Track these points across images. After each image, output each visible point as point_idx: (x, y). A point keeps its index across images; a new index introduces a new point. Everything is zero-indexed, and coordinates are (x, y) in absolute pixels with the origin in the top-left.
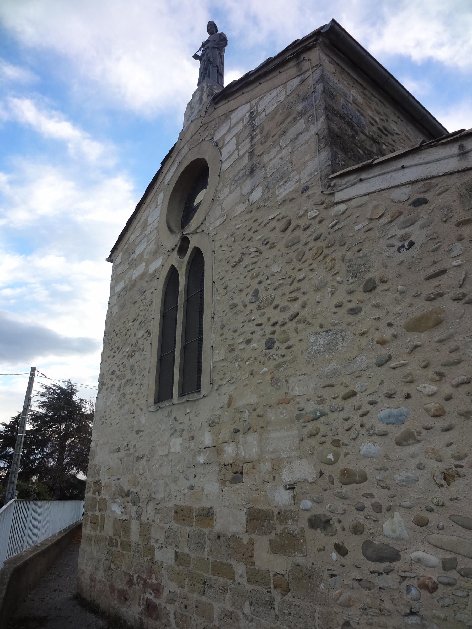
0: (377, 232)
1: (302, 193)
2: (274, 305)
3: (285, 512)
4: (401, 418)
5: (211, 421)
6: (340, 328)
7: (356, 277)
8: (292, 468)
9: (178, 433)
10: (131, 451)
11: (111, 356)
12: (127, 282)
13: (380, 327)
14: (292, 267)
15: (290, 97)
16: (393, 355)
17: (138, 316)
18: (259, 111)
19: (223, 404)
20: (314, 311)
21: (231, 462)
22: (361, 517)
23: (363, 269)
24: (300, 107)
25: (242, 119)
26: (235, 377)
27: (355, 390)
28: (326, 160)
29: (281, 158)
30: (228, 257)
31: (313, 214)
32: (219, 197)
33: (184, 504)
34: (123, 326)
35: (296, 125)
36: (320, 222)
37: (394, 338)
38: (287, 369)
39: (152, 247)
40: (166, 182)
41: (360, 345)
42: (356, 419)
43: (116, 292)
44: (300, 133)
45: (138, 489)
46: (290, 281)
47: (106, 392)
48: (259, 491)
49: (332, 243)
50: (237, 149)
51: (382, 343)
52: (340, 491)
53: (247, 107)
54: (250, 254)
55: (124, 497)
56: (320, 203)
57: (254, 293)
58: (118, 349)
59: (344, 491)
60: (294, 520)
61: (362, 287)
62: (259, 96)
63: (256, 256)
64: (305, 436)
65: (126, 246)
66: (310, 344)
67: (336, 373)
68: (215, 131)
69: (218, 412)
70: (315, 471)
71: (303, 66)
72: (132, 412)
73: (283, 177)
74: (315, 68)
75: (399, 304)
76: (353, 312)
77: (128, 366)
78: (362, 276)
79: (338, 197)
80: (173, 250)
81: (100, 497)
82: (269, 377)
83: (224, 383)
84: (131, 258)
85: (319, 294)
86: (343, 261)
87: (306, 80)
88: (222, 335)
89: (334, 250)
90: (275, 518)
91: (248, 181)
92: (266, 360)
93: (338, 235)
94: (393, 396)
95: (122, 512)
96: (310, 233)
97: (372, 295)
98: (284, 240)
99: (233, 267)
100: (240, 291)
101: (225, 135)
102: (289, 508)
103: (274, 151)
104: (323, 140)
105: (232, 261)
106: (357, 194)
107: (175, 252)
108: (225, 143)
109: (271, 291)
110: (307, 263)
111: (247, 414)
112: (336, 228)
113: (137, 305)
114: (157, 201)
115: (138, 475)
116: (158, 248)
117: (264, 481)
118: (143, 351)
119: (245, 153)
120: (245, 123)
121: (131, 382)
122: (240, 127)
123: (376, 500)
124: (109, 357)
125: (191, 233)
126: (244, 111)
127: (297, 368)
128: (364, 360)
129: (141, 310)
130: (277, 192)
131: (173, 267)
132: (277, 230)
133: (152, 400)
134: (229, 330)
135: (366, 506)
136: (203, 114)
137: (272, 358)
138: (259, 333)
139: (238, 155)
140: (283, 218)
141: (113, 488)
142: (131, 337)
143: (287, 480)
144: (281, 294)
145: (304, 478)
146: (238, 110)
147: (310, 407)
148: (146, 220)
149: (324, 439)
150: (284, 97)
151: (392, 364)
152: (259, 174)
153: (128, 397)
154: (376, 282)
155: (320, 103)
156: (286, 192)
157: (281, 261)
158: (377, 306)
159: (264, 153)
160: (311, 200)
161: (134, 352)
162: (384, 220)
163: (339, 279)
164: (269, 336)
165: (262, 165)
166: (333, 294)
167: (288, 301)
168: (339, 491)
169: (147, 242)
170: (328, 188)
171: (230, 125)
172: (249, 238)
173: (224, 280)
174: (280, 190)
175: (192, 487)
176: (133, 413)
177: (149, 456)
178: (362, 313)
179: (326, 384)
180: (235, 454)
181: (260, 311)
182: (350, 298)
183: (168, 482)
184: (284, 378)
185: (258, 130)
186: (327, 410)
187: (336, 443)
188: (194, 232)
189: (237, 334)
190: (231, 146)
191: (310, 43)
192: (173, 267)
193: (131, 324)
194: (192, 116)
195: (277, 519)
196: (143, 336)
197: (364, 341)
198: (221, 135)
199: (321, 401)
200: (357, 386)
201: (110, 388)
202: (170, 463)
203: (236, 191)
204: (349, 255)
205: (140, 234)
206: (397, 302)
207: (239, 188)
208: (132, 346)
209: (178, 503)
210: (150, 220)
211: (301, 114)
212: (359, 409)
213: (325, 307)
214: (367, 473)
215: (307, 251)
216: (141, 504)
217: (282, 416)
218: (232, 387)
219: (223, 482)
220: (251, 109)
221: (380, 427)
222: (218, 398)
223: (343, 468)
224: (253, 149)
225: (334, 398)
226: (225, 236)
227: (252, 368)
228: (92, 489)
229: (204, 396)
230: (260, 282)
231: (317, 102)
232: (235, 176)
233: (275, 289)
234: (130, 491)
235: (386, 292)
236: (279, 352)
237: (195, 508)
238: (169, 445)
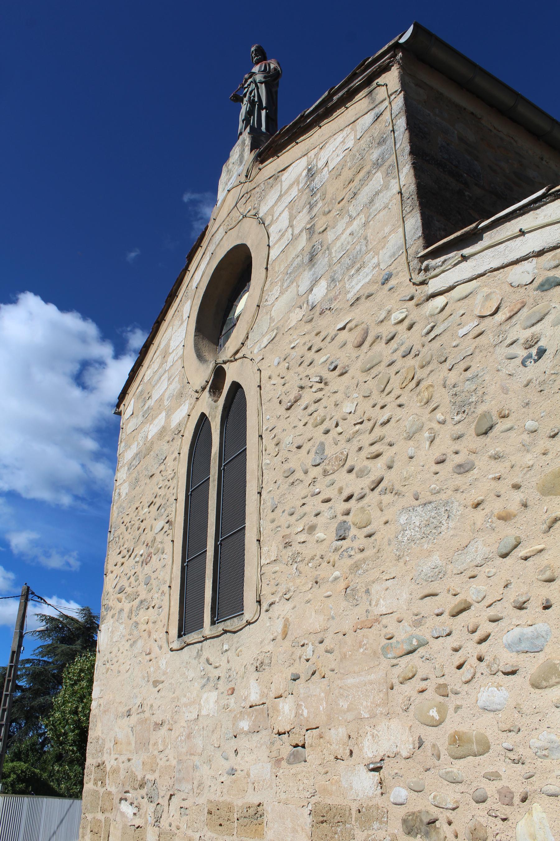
0: (491, 336)
1: (383, 284)
2: (347, 467)
3: (368, 808)
4: (538, 642)
5: (259, 662)
6: (443, 496)
7: (464, 412)
8: (377, 735)
9: (211, 684)
10: (147, 715)
11: (119, 564)
12: (141, 443)
13: (502, 492)
14: (372, 402)
15: (362, 142)
16: (523, 536)
17: (156, 497)
18: (319, 166)
19: (275, 634)
20: (405, 473)
21: (288, 729)
22: (481, 814)
23: (474, 399)
24: (375, 154)
25: (297, 181)
26: (292, 589)
27: (469, 600)
28: (414, 231)
29: (351, 234)
30: (279, 394)
31: (399, 315)
32: (266, 300)
33: (221, 799)
34: (136, 513)
35: (371, 182)
36: (410, 328)
37: (523, 507)
38: (367, 571)
39: (175, 386)
40: (194, 284)
41: (474, 524)
42: (471, 649)
43: (125, 462)
44: (377, 193)
45: (156, 775)
46: (369, 425)
47: (112, 621)
48: (329, 774)
49: (428, 359)
50: (291, 226)
51: (505, 518)
52: (450, 769)
53: (303, 162)
54: (311, 387)
55: (136, 789)
56: (408, 298)
57: (318, 449)
58: (128, 551)
59: (455, 771)
60: (381, 823)
61: (473, 427)
62: (319, 145)
63: (321, 390)
64: (395, 681)
65: (140, 388)
66: (400, 528)
67: (439, 574)
68: (260, 201)
69: (270, 647)
70: (411, 739)
71: (377, 94)
72: (148, 651)
73: (355, 263)
74: (393, 96)
75: (528, 451)
76: (462, 470)
77: (142, 578)
78: (472, 410)
79: (434, 285)
80: (204, 389)
81: (104, 789)
82: (342, 585)
83: (277, 600)
84: (146, 407)
85: (411, 443)
86: (445, 387)
87: (381, 114)
88: (273, 521)
89: (432, 371)
90: (353, 819)
91: (306, 272)
92: (336, 558)
93: (436, 344)
94: (525, 605)
95: (135, 814)
96: (395, 346)
97: (488, 439)
98: (359, 360)
99: (288, 409)
100: (299, 447)
101: (273, 206)
102: (374, 802)
103: (341, 224)
104: (409, 200)
105: (287, 400)
106: (458, 280)
107: (206, 393)
108: (275, 218)
109: (342, 444)
110: (393, 395)
111: (310, 648)
112: (432, 335)
113: (155, 479)
114: (182, 316)
115: (156, 753)
116: (183, 387)
117: (337, 758)
118: (163, 553)
119: (302, 231)
120: (301, 186)
121: (146, 604)
122: (294, 192)
123: (504, 783)
124: (116, 565)
125: (228, 361)
126: (298, 169)
127: (382, 569)
128: (481, 548)
129: (160, 488)
130: (347, 286)
131: (203, 415)
132: (350, 346)
133: (174, 631)
134: (283, 512)
135: (489, 794)
136: (243, 179)
137: (345, 553)
138: (327, 514)
139: (292, 234)
140: (356, 326)
141: (122, 774)
142: (146, 532)
143: (370, 755)
144: (357, 448)
145: (395, 750)
146: (291, 168)
147: (403, 634)
148: (168, 345)
149: (423, 685)
150: (353, 142)
151: (522, 552)
152: (322, 262)
153: (143, 627)
154: (494, 418)
155: (402, 147)
156: (360, 285)
157: (356, 395)
158: (496, 457)
159: (328, 229)
160: (396, 294)
161: (150, 555)
162: (501, 317)
163: (439, 416)
164: (341, 518)
165: (325, 247)
166: (432, 442)
167: (368, 458)
168: (447, 770)
169: (169, 380)
170: (419, 273)
171: (281, 191)
172: (310, 361)
173: (274, 431)
174: (351, 282)
175: (232, 772)
176: (149, 654)
177: (171, 722)
178: (475, 471)
179: (427, 592)
180: (293, 715)
181: (329, 478)
182: (456, 447)
183: (198, 764)
184: (364, 586)
185: (319, 195)
186: (428, 637)
187: (443, 691)
188: (232, 358)
189: (295, 517)
190: (283, 221)
191: (385, 61)
192: (203, 415)
193: (146, 510)
194: (229, 184)
195: (356, 821)
196: (162, 530)
197: (479, 516)
198: (269, 207)
199: (419, 621)
200: (471, 591)
201: (117, 615)
202: (201, 733)
203: (290, 290)
204: (453, 377)
205: (160, 367)
206: (526, 448)
207: (295, 284)
208: (147, 545)
209: (213, 797)
210: (173, 345)
211: (377, 165)
212: (474, 632)
213: (422, 464)
214: (489, 738)
215: (393, 376)
216: (160, 801)
217: (362, 650)
218: (290, 605)
219: (278, 761)
220: (308, 165)
221: (508, 659)
222: (268, 624)
223: (452, 731)
224: (312, 223)
225: (438, 615)
226: (276, 361)
227: (317, 573)
228: (92, 777)
229: (249, 623)
230: (327, 432)
231: (398, 146)
232: (288, 266)
233: (349, 440)
234: (146, 779)
235: (509, 433)
236: (357, 544)
237: (237, 806)
238: (200, 704)
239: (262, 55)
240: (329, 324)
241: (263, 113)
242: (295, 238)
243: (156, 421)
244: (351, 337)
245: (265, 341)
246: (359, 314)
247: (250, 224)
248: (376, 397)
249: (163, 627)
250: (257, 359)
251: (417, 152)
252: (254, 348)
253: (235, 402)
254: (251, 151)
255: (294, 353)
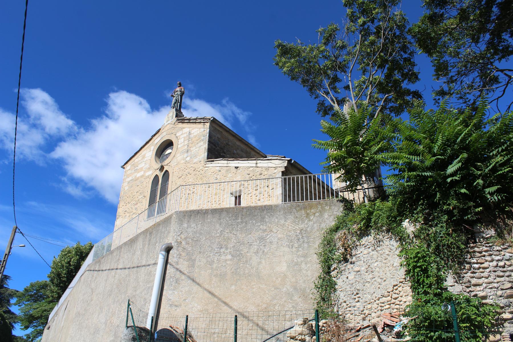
24: (202, 138)
39: (147, 166)
73: (196, 156)
79: (207, 166)
103: (194, 148)
122: (185, 135)
152: (189, 153)
240: (189, 165)
242: (184, 145)
244: (193, 169)
247: (173, 136)
249: (171, 327)
252: (173, 164)
253: (166, 175)
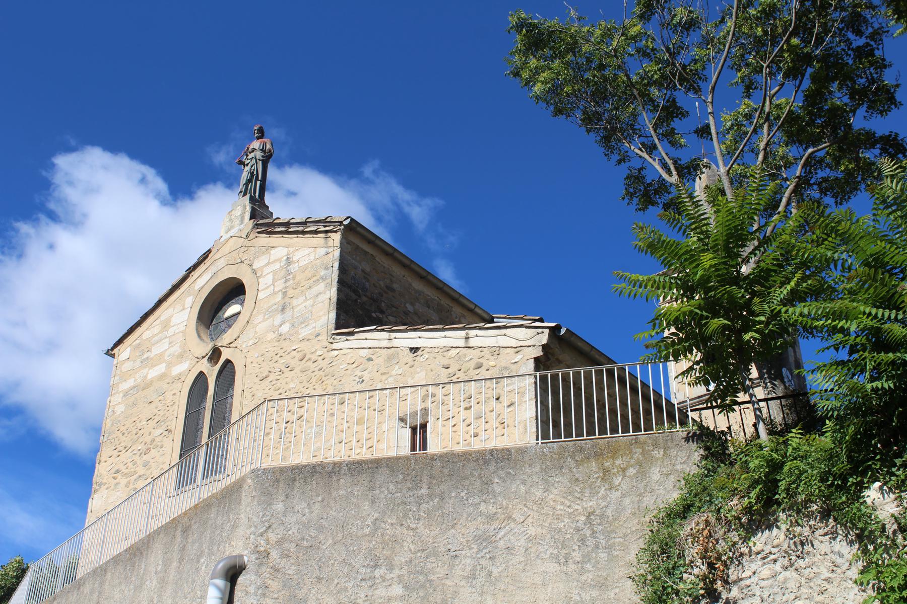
24: (323, 273)
39: (176, 349)
44: (320, 293)
73: (305, 322)
79: (335, 346)
80: (203, 357)
103: (301, 299)
113: (153, 405)
122: (277, 266)
152: (288, 313)
162: (354, 365)
204: (335, 383)
211: (323, 279)
239: (261, 134)
241: (258, 183)
242: (275, 293)
243: (156, 368)
244: (298, 356)
245: (251, 343)
246: (303, 346)
248: (305, 384)
250: (245, 351)
251: (340, 281)
253: (227, 372)
254: (251, 219)
255: (267, 354)
